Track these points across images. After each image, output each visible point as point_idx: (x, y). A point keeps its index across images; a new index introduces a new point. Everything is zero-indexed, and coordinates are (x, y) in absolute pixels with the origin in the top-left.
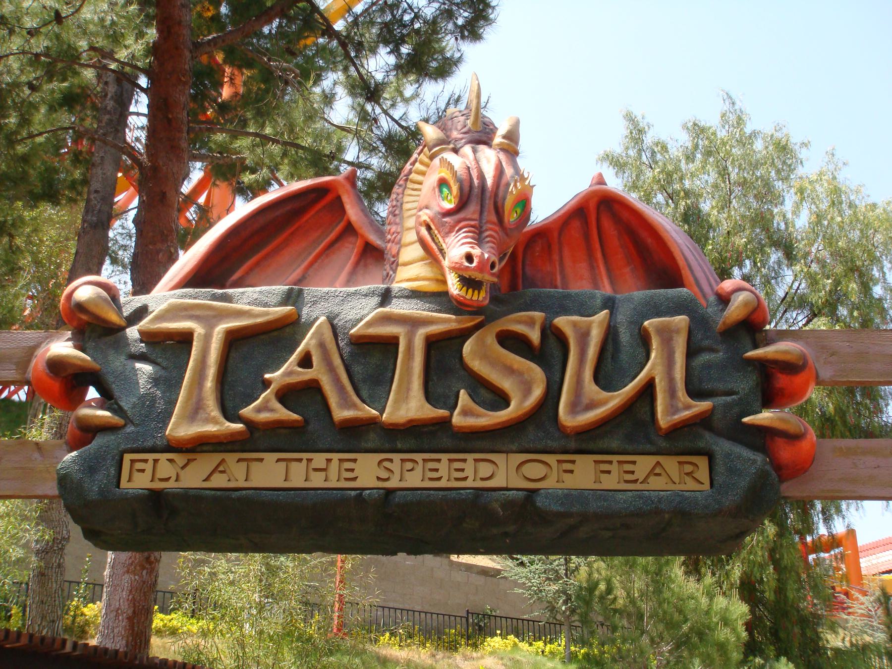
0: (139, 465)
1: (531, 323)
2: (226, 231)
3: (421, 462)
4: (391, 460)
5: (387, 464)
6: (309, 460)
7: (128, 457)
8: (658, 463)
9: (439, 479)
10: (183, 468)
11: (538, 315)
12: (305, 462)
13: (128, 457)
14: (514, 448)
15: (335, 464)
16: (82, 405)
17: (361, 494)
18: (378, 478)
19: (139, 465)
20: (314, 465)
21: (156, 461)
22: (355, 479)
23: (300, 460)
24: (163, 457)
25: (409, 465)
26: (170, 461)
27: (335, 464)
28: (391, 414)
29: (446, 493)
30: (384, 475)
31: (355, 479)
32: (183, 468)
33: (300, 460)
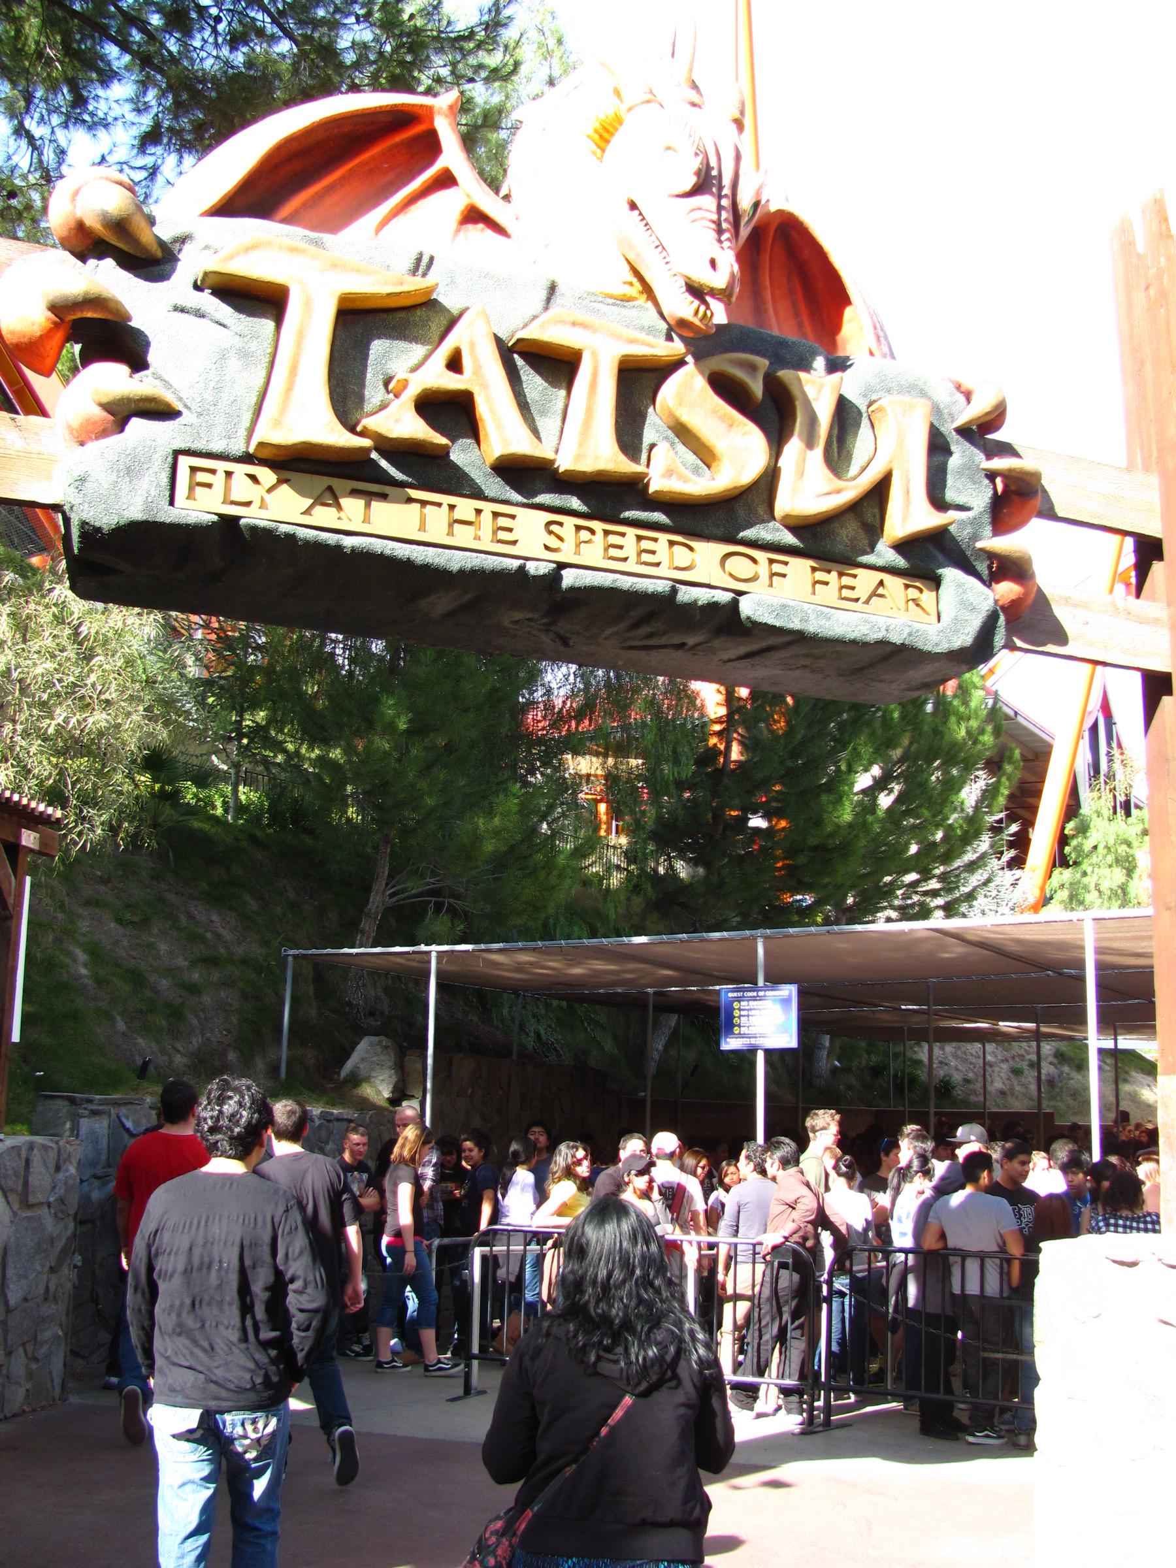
0: (201, 477)
1: (752, 368)
2: (352, 112)
3: (599, 534)
4: (561, 524)
5: (554, 528)
6: (452, 507)
7: (185, 462)
8: (881, 583)
9: (625, 559)
10: (270, 490)
11: (763, 363)
12: (445, 508)
13: (185, 462)
14: (719, 534)
15: (486, 517)
16: (392, 1166)
17: (522, 568)
18: (547, 548)
19: (201, 477)
20: (457, 514)
21: (229, 474)
22: (514, 543)
23: (439, 505)
24: (240, 469)
25: (585, 535)
26: (253, 478)
27: (486, 517)
28: (277, 423)
29: (617, 576)
30: (553, 542)
31: (514, 543)
32: (270, 490)
33: (439, 505)
